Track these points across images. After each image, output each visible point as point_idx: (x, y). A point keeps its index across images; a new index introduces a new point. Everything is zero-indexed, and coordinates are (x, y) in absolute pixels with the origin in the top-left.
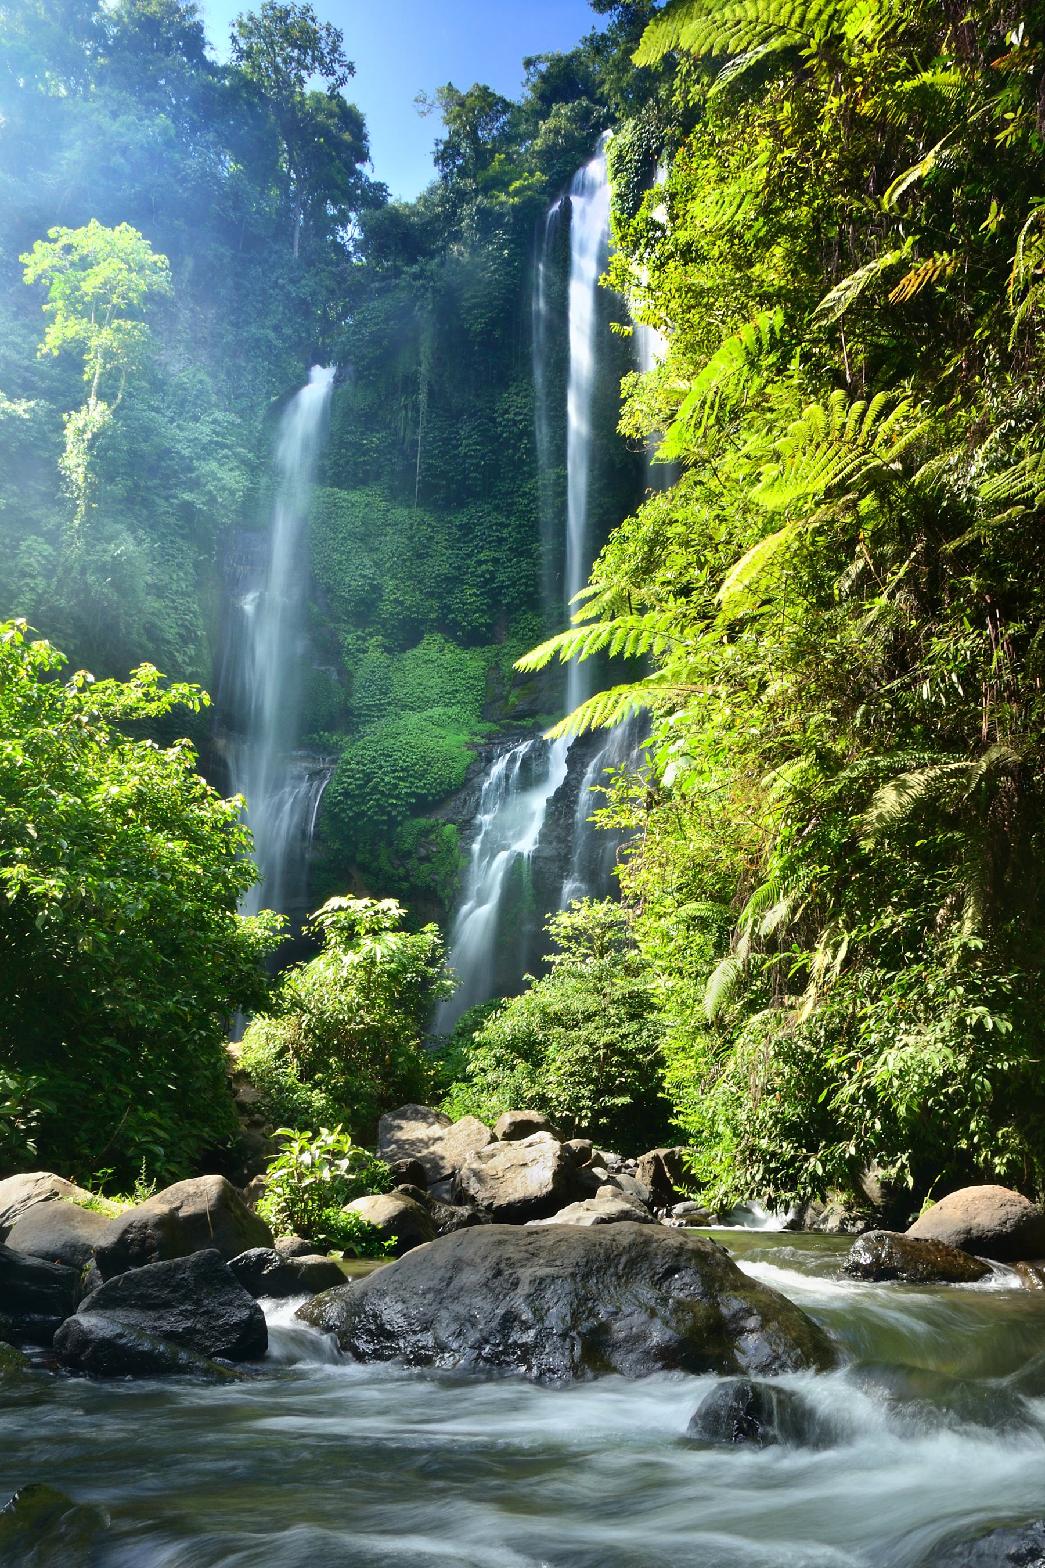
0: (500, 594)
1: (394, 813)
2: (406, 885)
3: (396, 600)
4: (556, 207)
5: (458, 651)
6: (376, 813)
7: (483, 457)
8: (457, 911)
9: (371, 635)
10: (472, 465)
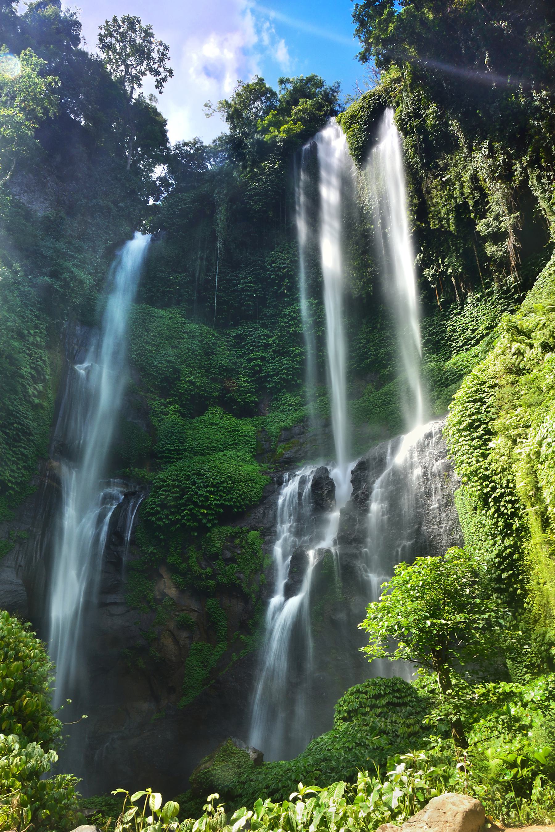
0: (266, 381)
1: (204, 521)
2: (212, 583)
3: (190, 381)
4: (307, 146)
5: (234, 419)
6: (188, 520)
7: (255, 291)
8: (266, 604)
9: (170, 403)
10: (247, 295)
